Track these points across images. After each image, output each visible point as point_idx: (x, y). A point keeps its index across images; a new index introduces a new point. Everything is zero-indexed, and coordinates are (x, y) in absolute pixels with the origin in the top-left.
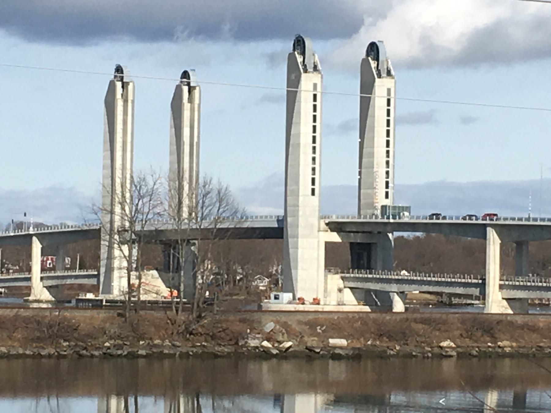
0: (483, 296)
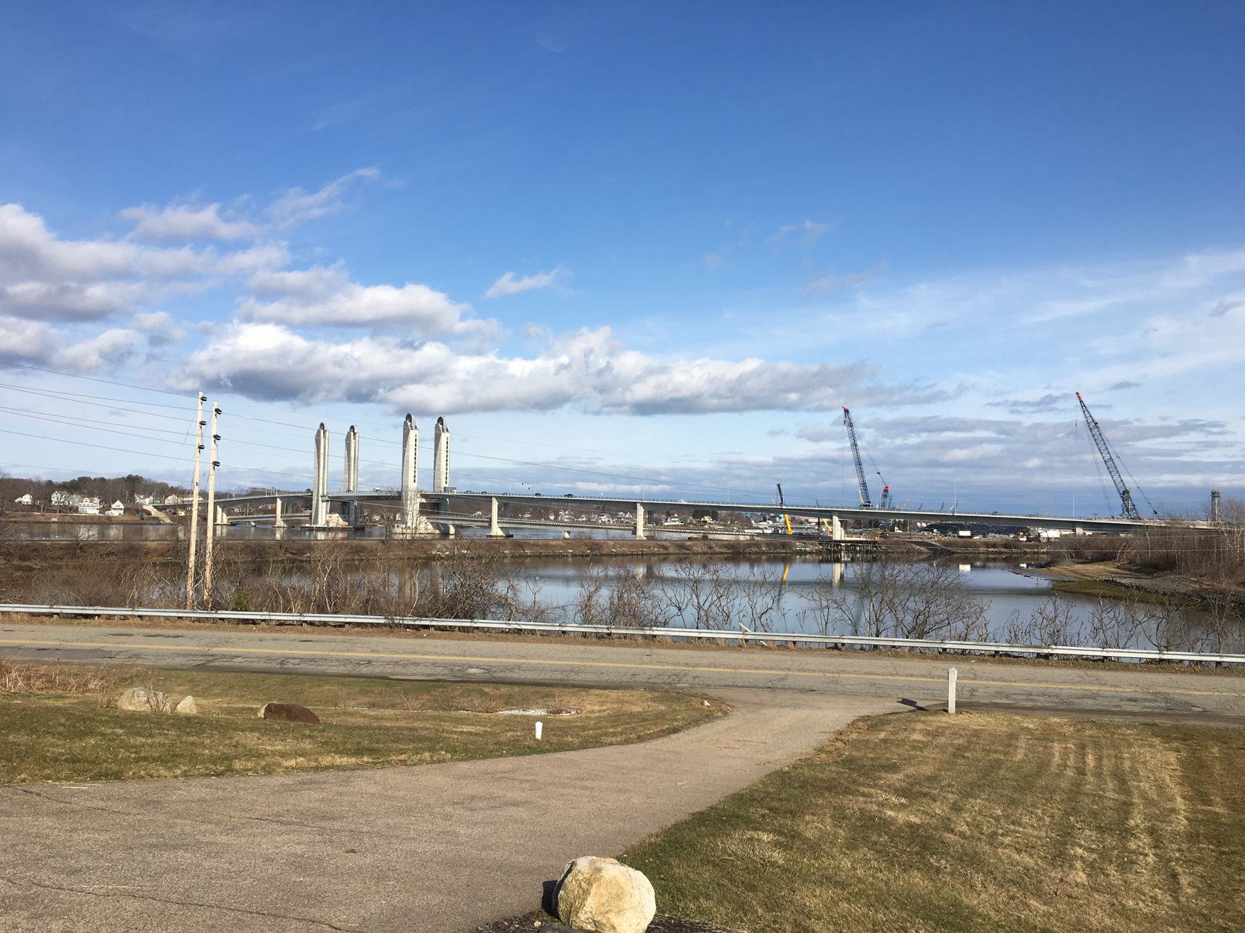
0: (490, 526)
